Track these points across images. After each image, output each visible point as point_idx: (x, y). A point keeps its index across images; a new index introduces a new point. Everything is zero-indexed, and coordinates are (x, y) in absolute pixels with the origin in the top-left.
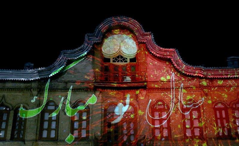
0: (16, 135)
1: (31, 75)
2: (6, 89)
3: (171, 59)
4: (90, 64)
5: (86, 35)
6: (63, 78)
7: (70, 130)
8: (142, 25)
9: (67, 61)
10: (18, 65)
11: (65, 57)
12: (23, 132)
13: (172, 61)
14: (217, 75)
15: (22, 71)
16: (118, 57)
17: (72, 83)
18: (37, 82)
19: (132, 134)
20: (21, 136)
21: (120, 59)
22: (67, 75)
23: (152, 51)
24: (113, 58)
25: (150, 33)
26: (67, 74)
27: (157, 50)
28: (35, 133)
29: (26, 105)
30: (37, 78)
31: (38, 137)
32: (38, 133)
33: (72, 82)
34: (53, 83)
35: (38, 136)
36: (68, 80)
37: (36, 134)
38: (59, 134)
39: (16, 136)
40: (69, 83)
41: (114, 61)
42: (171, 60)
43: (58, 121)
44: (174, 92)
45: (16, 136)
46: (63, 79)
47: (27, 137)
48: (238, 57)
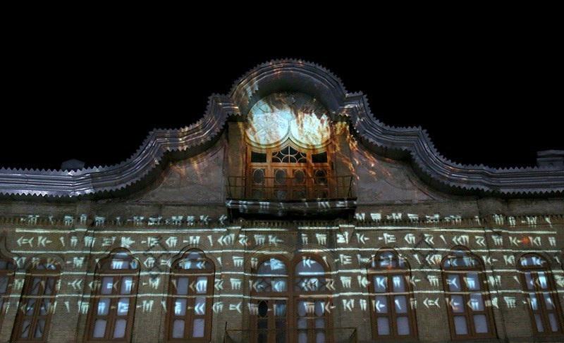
0: (28, 331)
1: (74, 180)
2: (10, 219)
3: (410, 152)
4: (219, 165)
5: (210, 98)
6: (153, 196)
7: (164, 318)
8: (341, 79)
9: (163, 155)
10: (46, 158)
11: (160, 145)
12: (46, 324)
13: (412, 156)
14: (521, 185)
15: (52, 174)
16: (286, 151)
17: (173, 207)
18: (89, 202)
19: (302, 330)
20: (39, 335)
21: (289, 155)
22: (163, 189)
23: (363, 135)
24: (274, 154)
25: (361, 93)
26: (165, 187)
27: (378, 133)
28: (75, 326)
29: (41, 220)
30: (88, 191)
31: (80, 337)
32: (83, 326)
33: (174, 205)
34: (127, 207)
35: (82, 332)
36: (164, 200)
37: (78, 329)
38: (136, 330)
39: (25, 335)
40: (166, 207)
41: (274, 160)
42: (411, 154)
43: (131, 317)
44: (329, 273)
45: (25, 335)
46: (152, 199)
47: (54, 337)
48: (562, 152)
